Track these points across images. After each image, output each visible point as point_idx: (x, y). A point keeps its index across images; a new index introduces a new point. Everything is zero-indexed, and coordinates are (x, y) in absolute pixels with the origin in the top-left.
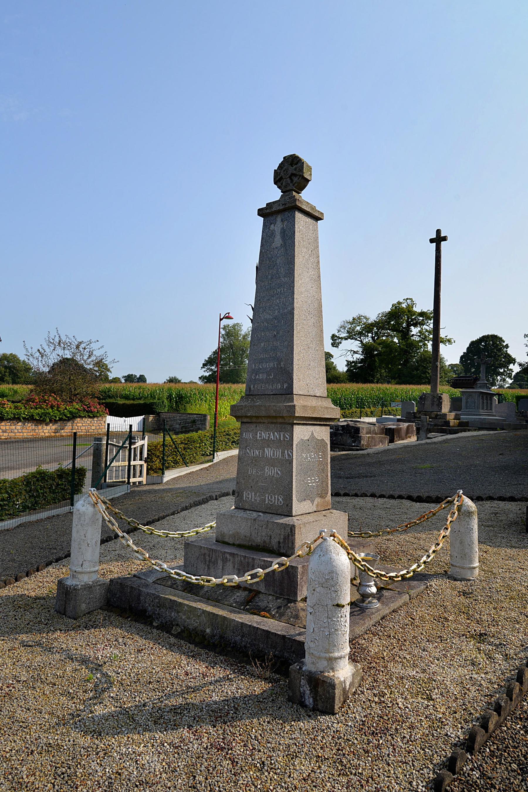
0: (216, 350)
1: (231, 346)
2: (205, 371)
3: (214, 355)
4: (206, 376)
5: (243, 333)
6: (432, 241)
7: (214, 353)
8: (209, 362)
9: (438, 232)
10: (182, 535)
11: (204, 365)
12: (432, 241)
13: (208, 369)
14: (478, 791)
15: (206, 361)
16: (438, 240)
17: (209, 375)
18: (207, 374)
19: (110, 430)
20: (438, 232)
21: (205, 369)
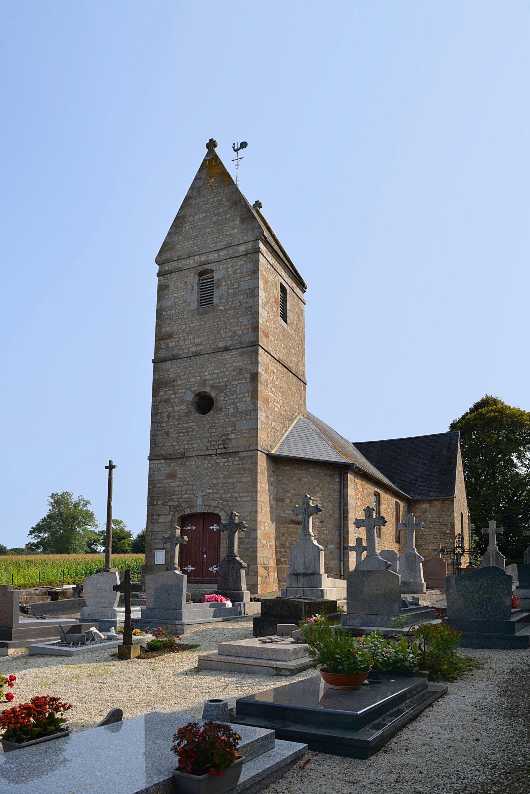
0: (45, 518)
1: (61, 514)
2: (32, 538)
3: (43, 522)
4: (34, 543)
5: (73, 501)
6: (106, 468)
7: (44, 520)
8: (38, 529)
9: (110, 462)
10: (358, 524)
11: (31, 532)
12: (106, 468)
13: (35, 536)
14: (84, 793)
15: (33, 528)
16: (110, 467)
17: (37, 542)
18: (35, 541)
19: (202, 522)
20: (110, 462)
21: (33, 536)
